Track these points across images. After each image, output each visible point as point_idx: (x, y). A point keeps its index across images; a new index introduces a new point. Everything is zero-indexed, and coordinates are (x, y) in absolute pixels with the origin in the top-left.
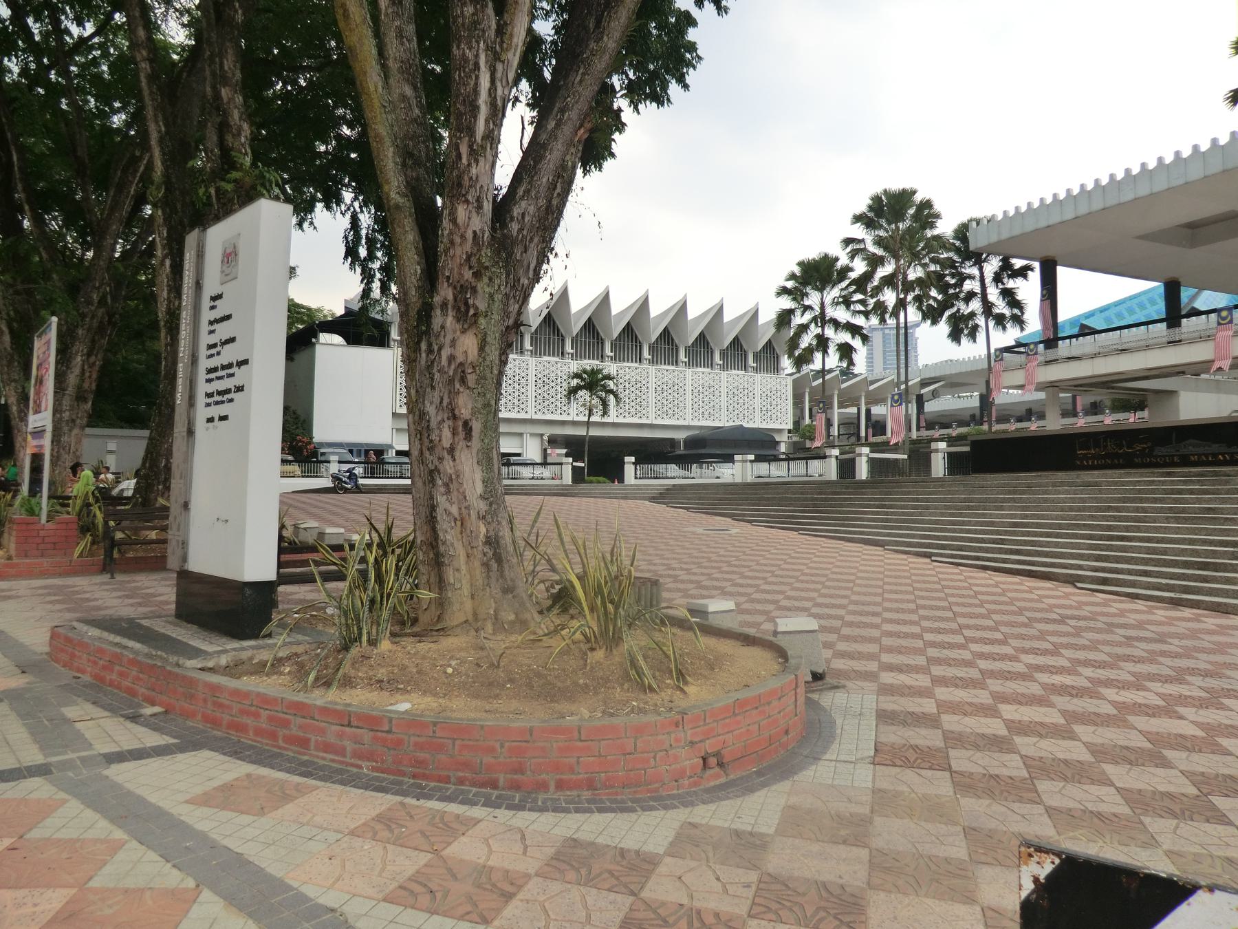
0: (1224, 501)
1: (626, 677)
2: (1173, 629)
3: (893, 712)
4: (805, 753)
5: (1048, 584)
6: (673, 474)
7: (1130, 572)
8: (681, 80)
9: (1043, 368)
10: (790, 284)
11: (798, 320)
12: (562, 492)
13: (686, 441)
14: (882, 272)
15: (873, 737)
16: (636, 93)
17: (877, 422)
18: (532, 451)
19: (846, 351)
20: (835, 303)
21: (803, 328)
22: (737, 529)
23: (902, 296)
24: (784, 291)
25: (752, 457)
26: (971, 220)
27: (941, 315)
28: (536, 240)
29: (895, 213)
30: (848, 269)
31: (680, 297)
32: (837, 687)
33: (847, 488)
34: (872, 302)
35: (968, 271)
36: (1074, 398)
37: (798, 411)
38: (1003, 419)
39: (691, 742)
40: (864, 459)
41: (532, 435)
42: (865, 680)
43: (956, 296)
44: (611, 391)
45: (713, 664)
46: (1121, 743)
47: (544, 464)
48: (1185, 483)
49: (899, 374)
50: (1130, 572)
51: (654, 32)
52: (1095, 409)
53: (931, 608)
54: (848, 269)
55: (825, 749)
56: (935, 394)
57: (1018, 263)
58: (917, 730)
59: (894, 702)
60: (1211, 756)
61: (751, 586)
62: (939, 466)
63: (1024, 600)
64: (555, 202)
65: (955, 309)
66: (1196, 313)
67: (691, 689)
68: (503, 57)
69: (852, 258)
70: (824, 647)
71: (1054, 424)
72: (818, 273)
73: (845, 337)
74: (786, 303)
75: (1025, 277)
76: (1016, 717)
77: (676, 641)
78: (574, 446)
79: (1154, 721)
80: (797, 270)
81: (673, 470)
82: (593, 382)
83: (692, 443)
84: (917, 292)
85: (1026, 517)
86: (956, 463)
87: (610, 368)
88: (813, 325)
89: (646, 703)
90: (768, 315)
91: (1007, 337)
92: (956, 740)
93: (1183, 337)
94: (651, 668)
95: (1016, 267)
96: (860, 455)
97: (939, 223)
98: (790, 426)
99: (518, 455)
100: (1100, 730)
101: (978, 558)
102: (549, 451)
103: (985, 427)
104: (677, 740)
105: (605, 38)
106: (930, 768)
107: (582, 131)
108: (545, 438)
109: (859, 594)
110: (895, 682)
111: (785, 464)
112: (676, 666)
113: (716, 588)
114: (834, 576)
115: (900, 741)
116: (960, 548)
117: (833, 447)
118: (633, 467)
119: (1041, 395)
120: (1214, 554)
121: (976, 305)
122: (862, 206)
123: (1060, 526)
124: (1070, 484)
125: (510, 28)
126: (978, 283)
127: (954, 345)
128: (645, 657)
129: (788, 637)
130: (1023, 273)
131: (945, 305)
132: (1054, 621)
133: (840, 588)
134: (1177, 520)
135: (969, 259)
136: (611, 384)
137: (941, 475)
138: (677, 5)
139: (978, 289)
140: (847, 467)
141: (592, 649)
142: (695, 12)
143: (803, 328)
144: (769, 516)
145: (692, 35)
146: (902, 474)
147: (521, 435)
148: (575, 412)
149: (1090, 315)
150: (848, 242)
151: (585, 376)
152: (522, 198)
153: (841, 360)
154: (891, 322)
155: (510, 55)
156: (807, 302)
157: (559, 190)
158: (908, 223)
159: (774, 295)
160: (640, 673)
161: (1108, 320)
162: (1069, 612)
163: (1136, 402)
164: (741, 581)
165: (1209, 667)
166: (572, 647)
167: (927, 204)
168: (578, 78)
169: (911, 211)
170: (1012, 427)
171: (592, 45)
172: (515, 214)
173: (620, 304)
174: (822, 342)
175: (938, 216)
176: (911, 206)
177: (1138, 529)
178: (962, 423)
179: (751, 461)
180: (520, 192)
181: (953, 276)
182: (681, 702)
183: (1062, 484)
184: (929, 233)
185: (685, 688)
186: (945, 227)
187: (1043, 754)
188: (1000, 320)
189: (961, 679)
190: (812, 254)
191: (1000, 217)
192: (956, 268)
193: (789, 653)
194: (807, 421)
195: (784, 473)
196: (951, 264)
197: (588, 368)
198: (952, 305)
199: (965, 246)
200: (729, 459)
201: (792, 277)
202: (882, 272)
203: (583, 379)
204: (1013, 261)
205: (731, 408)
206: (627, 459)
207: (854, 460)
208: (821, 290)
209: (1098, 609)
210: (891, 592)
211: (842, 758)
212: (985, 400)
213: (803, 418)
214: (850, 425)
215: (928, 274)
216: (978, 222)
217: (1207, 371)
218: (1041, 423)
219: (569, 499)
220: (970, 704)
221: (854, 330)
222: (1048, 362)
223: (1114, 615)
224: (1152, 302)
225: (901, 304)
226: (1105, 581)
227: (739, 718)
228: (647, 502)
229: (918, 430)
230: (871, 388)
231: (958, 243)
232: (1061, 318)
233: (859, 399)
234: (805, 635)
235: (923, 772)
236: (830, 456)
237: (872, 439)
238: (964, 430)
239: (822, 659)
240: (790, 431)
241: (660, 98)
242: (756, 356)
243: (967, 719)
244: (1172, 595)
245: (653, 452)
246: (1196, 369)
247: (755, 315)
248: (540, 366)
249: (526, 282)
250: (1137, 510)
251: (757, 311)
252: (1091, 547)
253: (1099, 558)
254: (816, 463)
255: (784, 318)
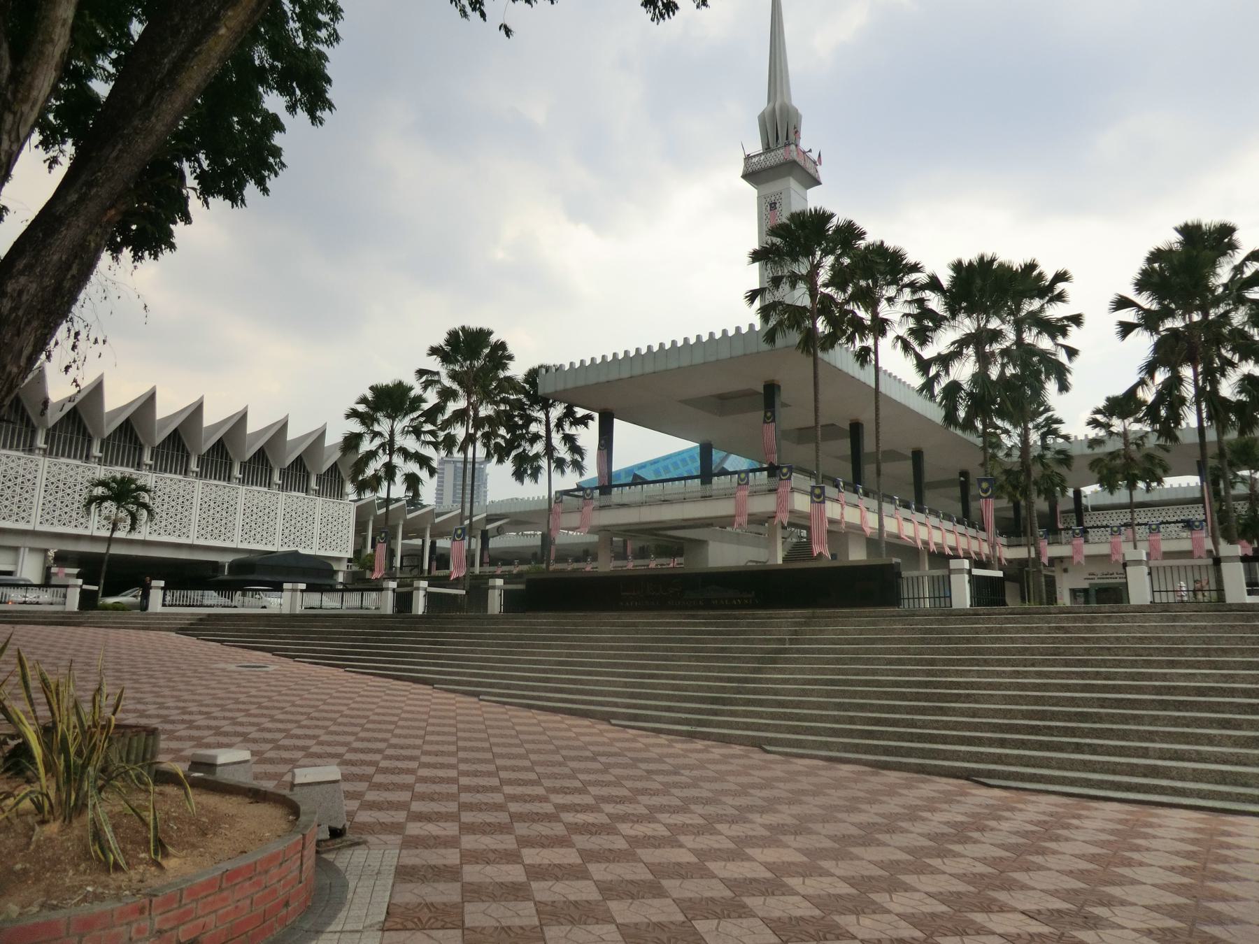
0: (734, 641)
1: (86, 855)
2: (686, 761)
3: (414, 867)
4: (307, 927)
5: (586, 722)
6: (212, 602)
7: (656, 708)
8: (261, 183)
9: (596, 513)
10: (362, 408)
11: (366, 446)
12: (64, 620)
13: (231, 565)
14: (452, 407)
15: (387, 899)
16: (208, 187)
17: (442, 556)
18: (30, 569)
19: (413, 482)
20: (405, 432)
21: (372, 455)
22: (275, 665)
23: (471, 431)
24: (353, 414)
25: (303, 586)
26: (541, 367)
27: (508, 455)
28: (35, 324)
29: (472, 353)
30: (420, 399)
31: (240, 408)
32: (358, 844)
33: (401, 622)
34: (441, 435)
35: (535, 414)
36: (625, 542)
37: (361, 540)
38: (561, 558)
39: (160, 932)
40: (422, 593)
41: (32, 550)
42: (391, 832)
43: (522, 437)
44: (145, 506)
45: (205, 828)
46: (628, 877)
47: (46, 584)
48: (705, 625)
49: (463, 508)
50: (656, 708)
51: (237, 127)
52: (642, 553)
53: (472, 749)
54: (420, 399)
55: (333, 917)
56: (500, 531)
57: (580, 412)
58: (436, 885)
59: (417, 856)
60: (699, 881)
61: (280, 730)
62: (495, 603)
63: (562, 738)
64: (67, 284)
65: (521, 450)
66: (724, 473)
67: (171, 864)
68: (16, 107)
69: (425, 388)
70: (346, 797)
71: (605, 565)
72: (390, 400)
73: (413, 467)
74: (355, 426)
75: (586, 425)
76: (537, 860)
77: (159, 804)
78: (89, 566)
79: (658, 852)
80: (370, 395)
81: (212, 597)
82: (123, 493)
83: (236, 567)
84: (486, 429)
85: (571, 655)
86: (513, 602)
87: (147, 478)
88: (381, 451)
89: (106, 886)
90: (334, 438)
91: (569, 480)
92: (474, 892)
93: (714, 493)
94: (121, 839)
95: (578, 415)
96: (418, 589)
97: (511, 364)
98: (350, 555)
99: (10, 573)
100: (612, 866)
101: (524, 697)
102: (54, 570)
103: (544, 566)
104: (139, 931)
105: (153, 119)
106: (443, 928)
107: (113, 212)
108: (51, 554)
109: (400, 736)
110: (422, 833)
111: (340, 594)
112: (155, 836)
113: (236, 734)
114: (376, 718)
115: (415, 900)
116: (508, 687)
117: (394, 579)
118: (161, 593)
119: (595, 538)
120: (723, 690)
121: (539, 447)
122: (440, 340)
123: (600, 665)
124: (613, 625)
125: (29, 78)
126: (544, 427)
127: (518, 484)
128: (115, 828)
129: (306, 789)
130: (584, 421)
131: (511, 445)
132: (587, 759)
133: (380, 731)
134: (698, 659)
135: (537, 403)
136: (145, 498)
137: (497, 612)
138: (265, 106)
139: (543, 433)
140: (404, 601)
141: (43, 822)
142: (284, 117)
143: (372, 455)
144: (315, 651)
145: (278, 139)
146: (460, 609)
147: (16, 549)
148: (96, 526)
149: (642, 466)
150: (421, 373)
151: (114, 485)
152: (22, 273)
153: (408, 489)
154: (457, 455)
155: (26, 108)
156: (377, 428)
157: (74, 271)
158: (481, 362)
159: (343, 416)
160: (104, 848)
161: (657, 472)
162: (601, 749)
163: (675, 548)
164: (270, 725)
165: (710, 795)
166: (16, 821)
167: (502, 346)
168: (114, 154)
169: (486, 351)
170: (569, 566)
171: (136, 122)
172: (9, 289)
173: (168, 407)
174: (390, 470)
175: (510, 358)
176: (486, 347)
177: (666, 668)
178: (523, 561)
179: (302, 591)
180: (21, 264)
181: (521, 417)
182: (154, 880)
183: (605, 624)
184: (502, 374)
185: (164, 863)
186: (517, 370)
187: (556, 898)
188: (560, 463)
189: (489, 824)
190: (387, 380)
191: (567, 367)
192: (524, 410)
193: (303, 808)
194: (369, 550)
195: (339, 605)
196: (518, 405)
197: (119, 476)
198: (519, 446)
199: (538, 391)
200: (278, 587)
201: (363, 400)
202: (452, 407)
203: (110, 489)
204: (576, 409)
205: (287, 531)
206: (154, 583)
207: (411, 594)
208: (392, 417)
209: (627, 745)
210: (433, 733)
211: (348, 927)
212: (547, 539)
213: (365, 546)
214: (413, 557)
215: (498, 412)
216: (547, 369)
217: (732, 525)
218: (595, 564)
219: (71, 629)
220: (494, 851)
221: (424, 461)
222: (602, 508)
223: (640, 750)
224: (692, 458)
225: (470, 439)
226: (635, 718)
227: (225, 894)
228: (173, 634)
229: (481, 565)
230: (437, 520)
231: (527, 386)
232: (616, 467)
233: (424, 530)
234: (326, 786)
235: (434, 933)
236: (387, 589)
237: (435, 573)
238: (525, 568)
239: (344, 810)
240: (350, 560)
241: (234, 196)
242: (319, 478)
243: (488, 867)
244: (688, 728)
245: (187, 575)
246: (724, 522)
247: (322, 435)
248: (54, 468)
249: (15, 370)
250: (666, 649)
251: (324, 432)
252: (626, 685)
253: (632, 696)
254: (374, 595)
255: (352, 441)
